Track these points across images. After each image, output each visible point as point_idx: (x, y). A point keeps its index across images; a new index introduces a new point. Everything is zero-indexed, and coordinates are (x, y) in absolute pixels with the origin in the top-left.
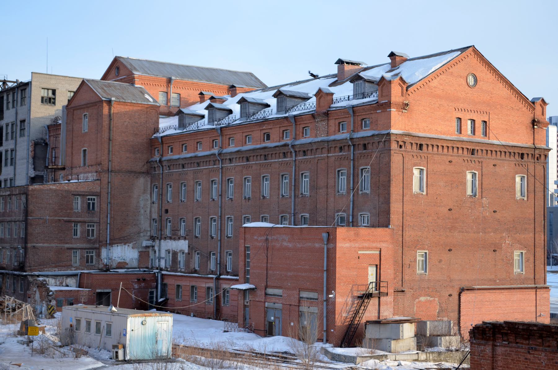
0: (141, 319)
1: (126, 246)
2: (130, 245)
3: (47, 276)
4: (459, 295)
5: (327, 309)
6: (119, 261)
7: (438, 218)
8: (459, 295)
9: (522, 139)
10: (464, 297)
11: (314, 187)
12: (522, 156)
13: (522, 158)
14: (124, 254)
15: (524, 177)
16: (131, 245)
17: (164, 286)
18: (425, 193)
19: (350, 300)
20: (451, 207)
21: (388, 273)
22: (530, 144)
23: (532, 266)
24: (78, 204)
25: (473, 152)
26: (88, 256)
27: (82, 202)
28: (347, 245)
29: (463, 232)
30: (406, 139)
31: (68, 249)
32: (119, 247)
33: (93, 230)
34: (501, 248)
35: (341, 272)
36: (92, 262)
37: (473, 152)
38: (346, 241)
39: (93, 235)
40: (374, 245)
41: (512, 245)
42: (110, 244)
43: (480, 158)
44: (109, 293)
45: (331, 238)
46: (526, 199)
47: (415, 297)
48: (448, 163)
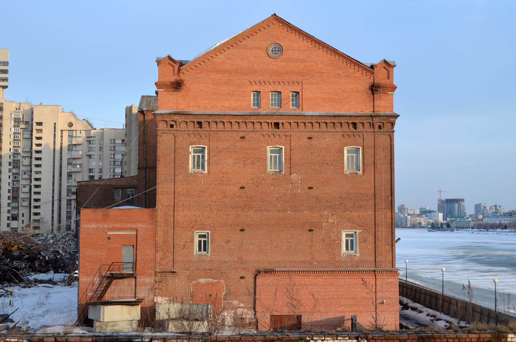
4: (255, 278)
7: (226, 197)
8: (255, 278)
9: (359, 106)
12: (355, 125)
13: (201, 127)
18: (206, 172)
19: (97, 280)
20: (244, 185)
21: (146, 252)
22: (369, 111)
23: (371, 247)
25: (277, 125)
29: (261, 211)
30: (176, 118)
34: (322, 228)
37: (277, 125)
40: (129, 226)
43: (288, 132)
46: (361, 172)
47: (190, 278)
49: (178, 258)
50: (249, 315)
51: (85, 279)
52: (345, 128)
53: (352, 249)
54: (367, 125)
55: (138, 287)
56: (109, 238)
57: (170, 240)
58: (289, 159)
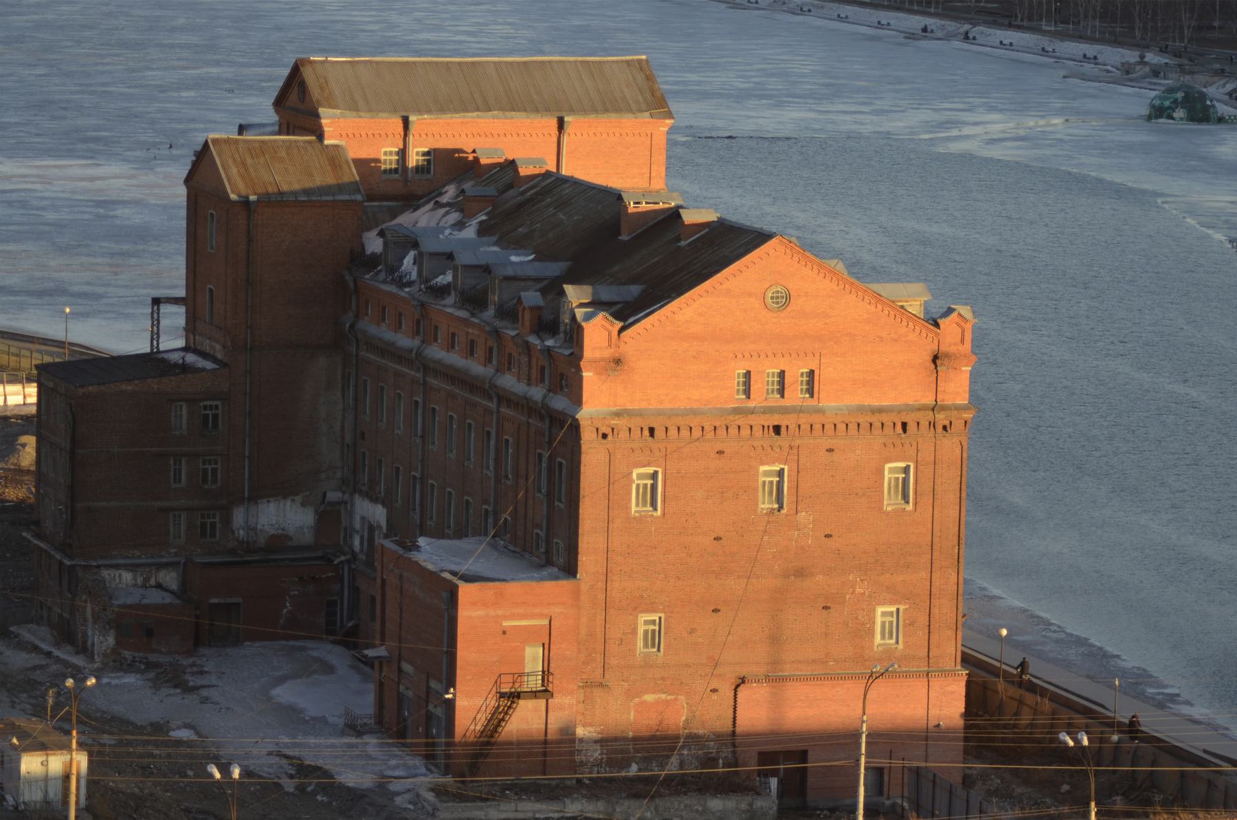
1: (289, 503)
2: (297, 498)
3: (117, 567)
6: (272, 532)
14: (286, 517)
16: (298, 499)
23: (922, 634)
24: (182, 417)
25: (777, 430)
26: (203, 525)
28: (480, 613)
32: (272, 504)
33: (214, 471)
36: (213, 535)
39: (215, 481)
40: (537, 610)
41: (870, 596)
44: (238, 605)
46: (910, 507)
47: (630, 694)
48: (713, 455)
51: (466, 703)
53: (653, 646)
56: (504, 633)
57: (600, 635)
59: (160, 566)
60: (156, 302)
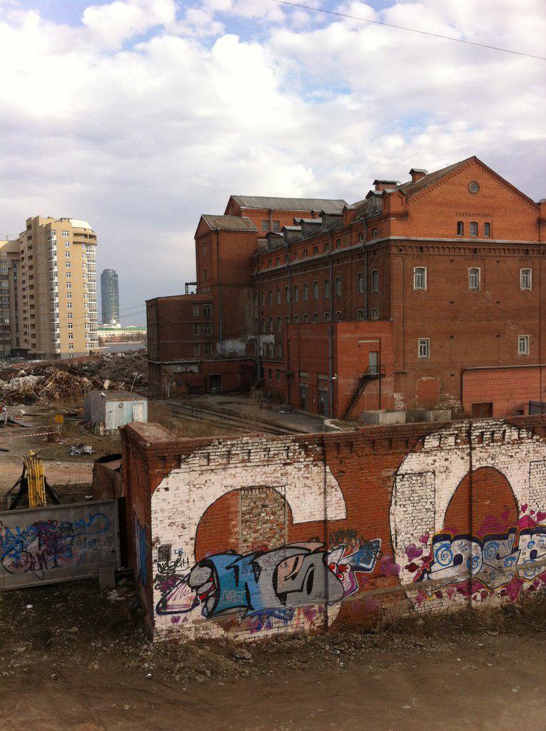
0: (118, 403)
5: (333, 388)
10: (465, 377)
11: (344, 289)
14: (235, 346)
15: (424, 269)
17: (262, 369)
21: (388, 358)
27: (200, 310)
31: (191, 343)
35: (342, 359)
38: (346, 335)
40: (374, 335)
42: (222, 339)
45: (333, 332)
47: (416, 377)
48: (449, 262)
49: (408, 361)
50: (458, 404)
52: (522, 254)
54: (535, 252)
55: (382, 386)
58: (484, 280)
59: (193, 364)
60: (187, 284)
